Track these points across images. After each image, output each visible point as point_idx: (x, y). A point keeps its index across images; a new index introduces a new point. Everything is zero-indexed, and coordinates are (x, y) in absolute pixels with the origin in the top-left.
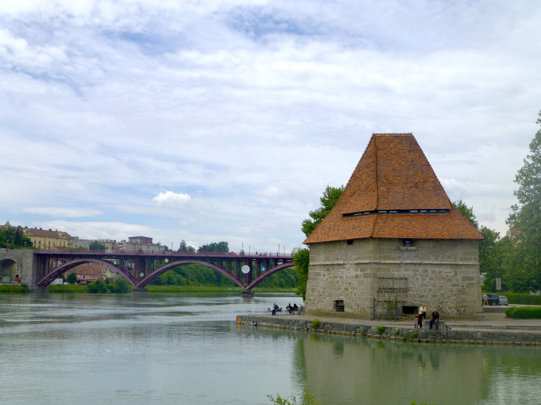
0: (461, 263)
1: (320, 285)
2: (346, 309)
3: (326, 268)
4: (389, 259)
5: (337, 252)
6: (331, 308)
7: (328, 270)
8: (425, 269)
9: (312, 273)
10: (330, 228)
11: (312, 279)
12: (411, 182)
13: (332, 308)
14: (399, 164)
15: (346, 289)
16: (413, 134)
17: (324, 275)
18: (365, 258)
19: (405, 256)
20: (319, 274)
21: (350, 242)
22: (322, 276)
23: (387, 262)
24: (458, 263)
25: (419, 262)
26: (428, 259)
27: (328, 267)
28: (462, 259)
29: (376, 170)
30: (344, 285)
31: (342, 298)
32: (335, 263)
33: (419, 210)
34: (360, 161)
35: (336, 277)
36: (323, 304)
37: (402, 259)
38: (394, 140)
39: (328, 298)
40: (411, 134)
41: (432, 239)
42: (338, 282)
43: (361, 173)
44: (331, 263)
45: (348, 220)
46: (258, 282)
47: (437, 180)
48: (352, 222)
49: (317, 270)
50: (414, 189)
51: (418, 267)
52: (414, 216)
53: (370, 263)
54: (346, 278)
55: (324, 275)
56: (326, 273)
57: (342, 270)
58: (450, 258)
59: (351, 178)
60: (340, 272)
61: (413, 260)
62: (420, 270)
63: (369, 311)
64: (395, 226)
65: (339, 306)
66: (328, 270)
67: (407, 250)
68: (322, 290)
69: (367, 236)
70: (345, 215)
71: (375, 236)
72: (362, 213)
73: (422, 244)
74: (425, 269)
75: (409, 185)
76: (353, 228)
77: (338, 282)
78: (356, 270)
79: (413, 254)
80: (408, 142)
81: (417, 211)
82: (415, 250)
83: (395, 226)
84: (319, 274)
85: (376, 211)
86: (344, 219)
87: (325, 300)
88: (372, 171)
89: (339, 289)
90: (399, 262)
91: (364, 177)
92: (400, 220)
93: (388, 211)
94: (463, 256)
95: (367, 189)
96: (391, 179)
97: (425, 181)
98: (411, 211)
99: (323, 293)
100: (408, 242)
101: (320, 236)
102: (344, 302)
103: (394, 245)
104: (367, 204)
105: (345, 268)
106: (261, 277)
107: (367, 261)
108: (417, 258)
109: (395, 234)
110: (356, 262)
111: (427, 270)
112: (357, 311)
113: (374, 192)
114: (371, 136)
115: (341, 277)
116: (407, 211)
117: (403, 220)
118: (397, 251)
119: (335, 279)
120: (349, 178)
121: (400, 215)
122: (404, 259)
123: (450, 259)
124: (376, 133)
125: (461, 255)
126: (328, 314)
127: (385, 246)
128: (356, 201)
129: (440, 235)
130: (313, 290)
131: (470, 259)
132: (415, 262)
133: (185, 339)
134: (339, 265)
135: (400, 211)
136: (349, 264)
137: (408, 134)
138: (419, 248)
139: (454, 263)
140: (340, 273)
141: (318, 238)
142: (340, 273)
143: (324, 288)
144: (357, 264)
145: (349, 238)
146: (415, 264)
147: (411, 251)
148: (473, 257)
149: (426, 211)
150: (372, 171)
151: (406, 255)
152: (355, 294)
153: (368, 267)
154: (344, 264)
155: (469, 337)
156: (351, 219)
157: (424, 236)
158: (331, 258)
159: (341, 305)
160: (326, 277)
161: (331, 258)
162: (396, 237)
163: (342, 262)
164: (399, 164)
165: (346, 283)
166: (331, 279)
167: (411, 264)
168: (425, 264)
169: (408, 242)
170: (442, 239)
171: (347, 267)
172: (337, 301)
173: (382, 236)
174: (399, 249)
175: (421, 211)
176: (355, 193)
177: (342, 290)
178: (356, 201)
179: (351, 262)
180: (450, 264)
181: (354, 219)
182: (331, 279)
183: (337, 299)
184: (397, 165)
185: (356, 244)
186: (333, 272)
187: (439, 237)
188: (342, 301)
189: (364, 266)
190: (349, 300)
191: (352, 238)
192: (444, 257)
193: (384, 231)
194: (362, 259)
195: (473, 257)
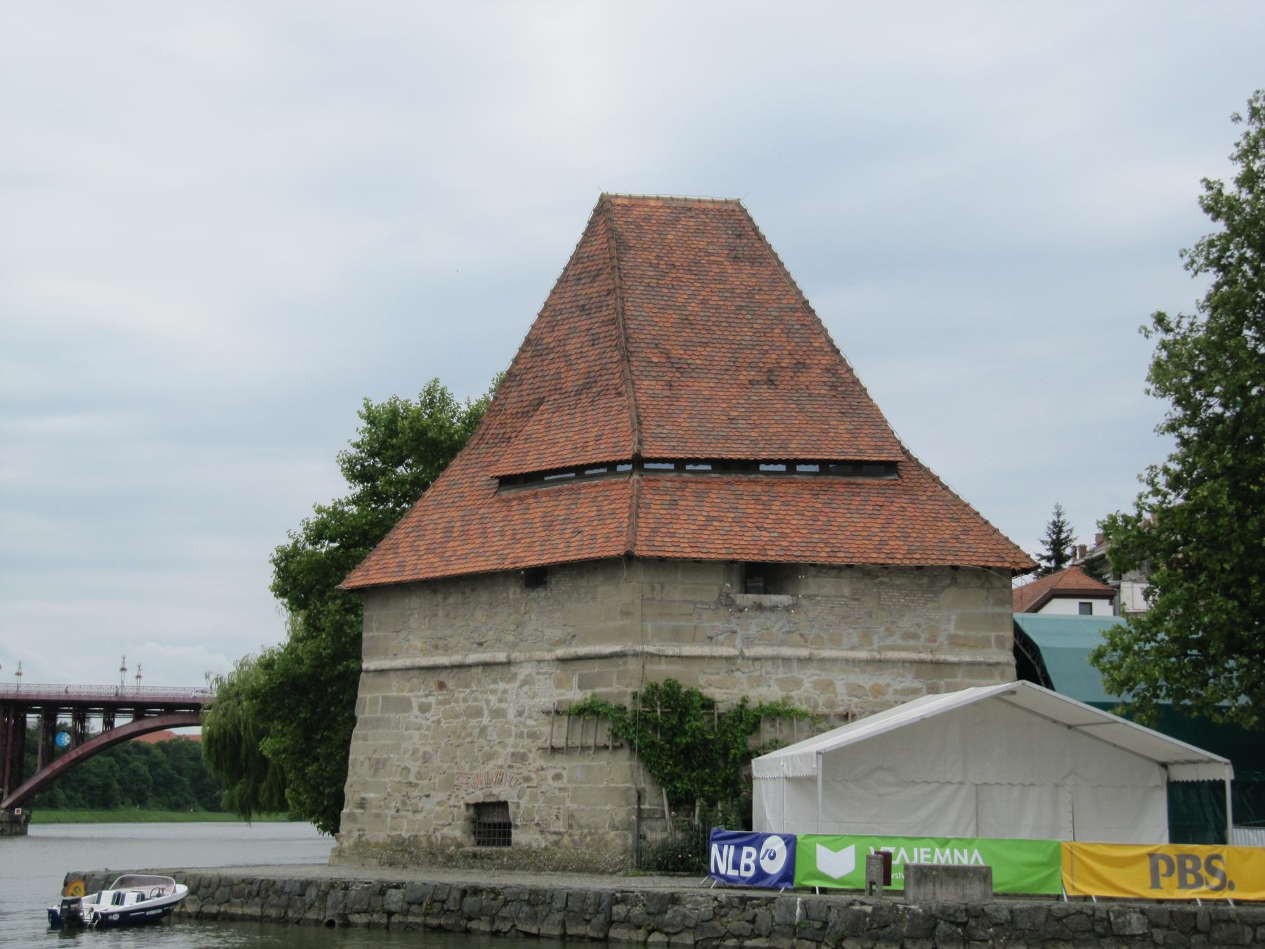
0: (952, 658)
1: (407, 745)
2: (517, 836)
3: (432, 680)
4: (694, 640)
5: (480, 615)
6: (456, 831)
7: (441, 686)
8: (824, 676)
9: (374, 701)
10: (448, 530)
11: (377, 723)
12: (751, 366)
13: (458, 833)
14: (704, 302)
15: (521, 757)
16: (744, 204)
17: (424, 708)
18: (602, 638)
19: (753, 630)
20: (404, 705)
21: (536, 577)
22: (416, 711)
23: (688, 650)
24: (942, 657)
25: (804, 652)
26: (836, 642)
27: (443, 676)
28: (955, 642)
29: (619, 321)
30: (511, 741)
31: (502, 792)
32: (473, 658)
33: (791, 464)
34: (553, 292)
35: (479, 713)
36: (420, 816)
37: (738, 641)
38: (678, 220)
39: (441, 796)
40: (738, 204)
41: (850, 566)
42: (483, 730)
43: (561, 332)
44: (456, 659)
45: (521, 499)
46: (44, 785)
47: (842, 361)
48: (538, 506)
49: (395, 689)
50: (765, 392)
51: (796, 672)
52: (774, 484)
53: (622, 655)
54: (520, 714)
55: (424, 708)
56: (431, 699)
57: (502, 686)
58: (914, 636)
59: (522, 350)
60: (493, 692)
61: (782, 644)
62: (807, 685)
63: (618, 841)
64: (710, 519)
65: (491, 823)
66: (441, 686)
67: (760, 607)
68: (414, 767)
69: (615, 549)
70: (507, 481)
71: (642, 550)
72: (580, 470)
73: (812, 586)
74: (824, 676)
75: (744, 376)
76: (548, 527)
77: (483, 730)
78: (559, 684)
79: (777, 623)
80: (731, 230)
81: (782, 468)
82: (787, 609)
83: (710, 519)
84: (404, 705)
85: (638, 462)
86: (505, 494)
87: (428, 805)
88: (605, 323)
89: (490, 757)
90: (732, 651)
91: (573, 345)
92: (742, 492)
93: (680, 464)
94: (961, 633)
95: (586, 387)
96: (677, 352)
97: (800, 366)
98: (763, 467)
99: (419, 775)
100: (763, 576)
101: (411, 560)
102: (511, 808)
103: (712, 587)
104: (598, 438)
105: (513, 678)
106: (58, 764)
107: (607, 649)
108: (796, 637)
109: (717, 547)
110: (560, 652)
111: (831, 684)
112: (566, 840)
113: (620, 394)
114: (594, 202)
115: (498, 714)
116: (747, 466)
117: (740, 497)
118: (722, 611)
119: (473, 722)
120: (514, 352)
121: (726, 478)
122: (748, 641)
123: (912, 643)
124: (612, 192)
125: (952, 630)
126: (439, 856)
127: (677, 590)
128: (548, 428)
129: (879, 551)
130: (378, 765)
131: (985, 643)
132: (786, 651)
133: (180, 926)
134: (486, 665)
135: (723, 466)
136: (529, 660)
137: (727, 202)
138: (804, 602)
139: (927, 656)
140: (493, 699)
141: (402, 565)
142: (493, 699)
143: (426, 758)
144: (563, 661)
145: (532, 561)
146: (787, 660)
147: (773, 608)
148: (993, 634)
149: (815, 468)
150: (605, 323)
151: (754, 625)
152: (558, 777)
153: (612, 669)
154: (509, 663)
155: (1099, 929)
156: (535, 496)
157: (822, 557)
158: (452, 642)
159: (496, 819)
160: (435, 713)
161: (452, 642)
162: (723, 555)
163: (502, 657)
164: (704, 302)
165: (521, 735)
166: (455, 723)
167: (773, 658)
168: (822, 660)
169: (763, 576)
170: (885, 567)
171: (523, 672)
172: (480, 808)
173: (669, 552)
174: (730, 603)
175: (800, 468)
176: (541, 401)
177: (500, 762)
178: (548, 428)
179: (539, 655)
180: (912, 662)
181: (547, 494)
182: (455, 723)
183: (479, 796)
184: (694, 306)
185: (560, 587)
186: (462, 693)
187: (876, 558)
188: (503, 805)
189: (596, 667)
190: (534, 798)
191: (546, 559)
192: (890, 633)
193: (672, 535)
194: (584, 642)
195: (993, 634)
